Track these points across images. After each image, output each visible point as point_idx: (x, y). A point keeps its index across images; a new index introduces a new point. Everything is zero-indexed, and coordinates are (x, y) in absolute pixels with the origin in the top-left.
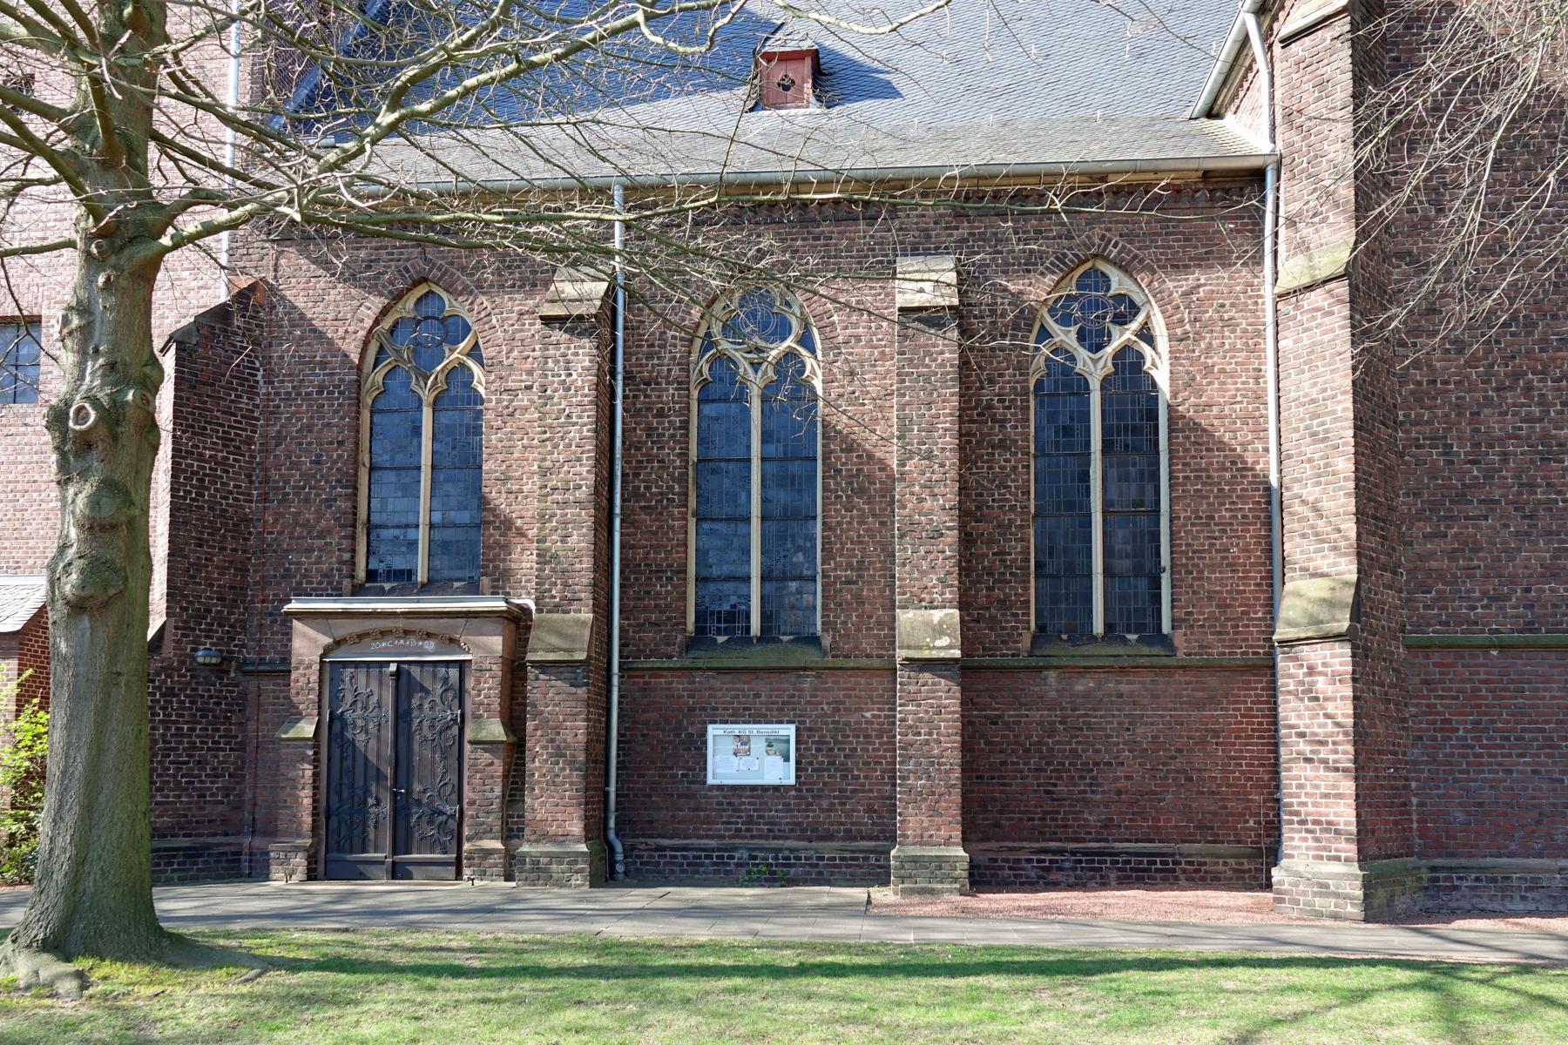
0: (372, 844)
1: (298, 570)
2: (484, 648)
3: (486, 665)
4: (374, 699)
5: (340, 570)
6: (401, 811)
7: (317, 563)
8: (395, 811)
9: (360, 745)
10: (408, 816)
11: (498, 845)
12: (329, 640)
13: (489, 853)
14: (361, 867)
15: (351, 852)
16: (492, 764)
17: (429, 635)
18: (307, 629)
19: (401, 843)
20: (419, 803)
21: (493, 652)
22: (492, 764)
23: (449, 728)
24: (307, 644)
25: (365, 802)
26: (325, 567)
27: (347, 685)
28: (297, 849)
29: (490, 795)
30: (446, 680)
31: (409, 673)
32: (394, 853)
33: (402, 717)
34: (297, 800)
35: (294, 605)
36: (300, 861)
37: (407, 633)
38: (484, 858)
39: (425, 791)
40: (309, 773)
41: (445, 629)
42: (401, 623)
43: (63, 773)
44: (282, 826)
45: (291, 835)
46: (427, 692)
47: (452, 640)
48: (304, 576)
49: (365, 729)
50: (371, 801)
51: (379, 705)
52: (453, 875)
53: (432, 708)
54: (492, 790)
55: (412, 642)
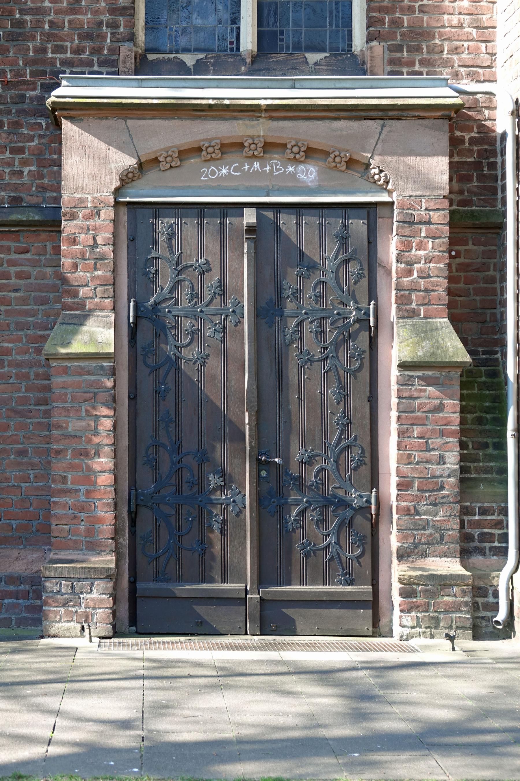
0: (217, 566)
1: (38, 24)
2: (418, 178)
3: (420, 214)
4: (213, 278)
5: (113, 25)
6: (270, 501)
7: (72, 11)
8: (261, 500)
9: (189, 370)
10: (284, 506)
11: (452, 566)
12: (130, 161)
13: (444, 582)
14: (202, 611)
15: (180, 580)
16: (440, 408)
17: (310, 153)
18: (89, 139)
19: (273, 565)
20: (300, 483)
21: (431, 186)
22: (440, 408)
23: (351, 336)
24: (90, 168)
25: (203, 479)
26: (86, 18)
27: (162, 250)
28: (91, 576)
29: (438, 469)
30: (344, 239)
31: (277, 229)
32: (262, 579)
33: (269, 312)
34: (89, 477)
35: (67, 91)
36: (98, 598)
37: (269, 147)
38: (432, 595)
39: (310, 461)
40: (108, 423)
41: (342, 137)
42: (262, 129)
43: (198, 732)
44: (59, 528)
45: (75, 546)
46: (312, 267)
47: (351, 163)
48: (49, 37)
49: (197, 335)
50: (214, 480)
51: (221, 290)
52: (368, 627)
53: (319, 297)
54: (441, 460)
55: (276, 166)
